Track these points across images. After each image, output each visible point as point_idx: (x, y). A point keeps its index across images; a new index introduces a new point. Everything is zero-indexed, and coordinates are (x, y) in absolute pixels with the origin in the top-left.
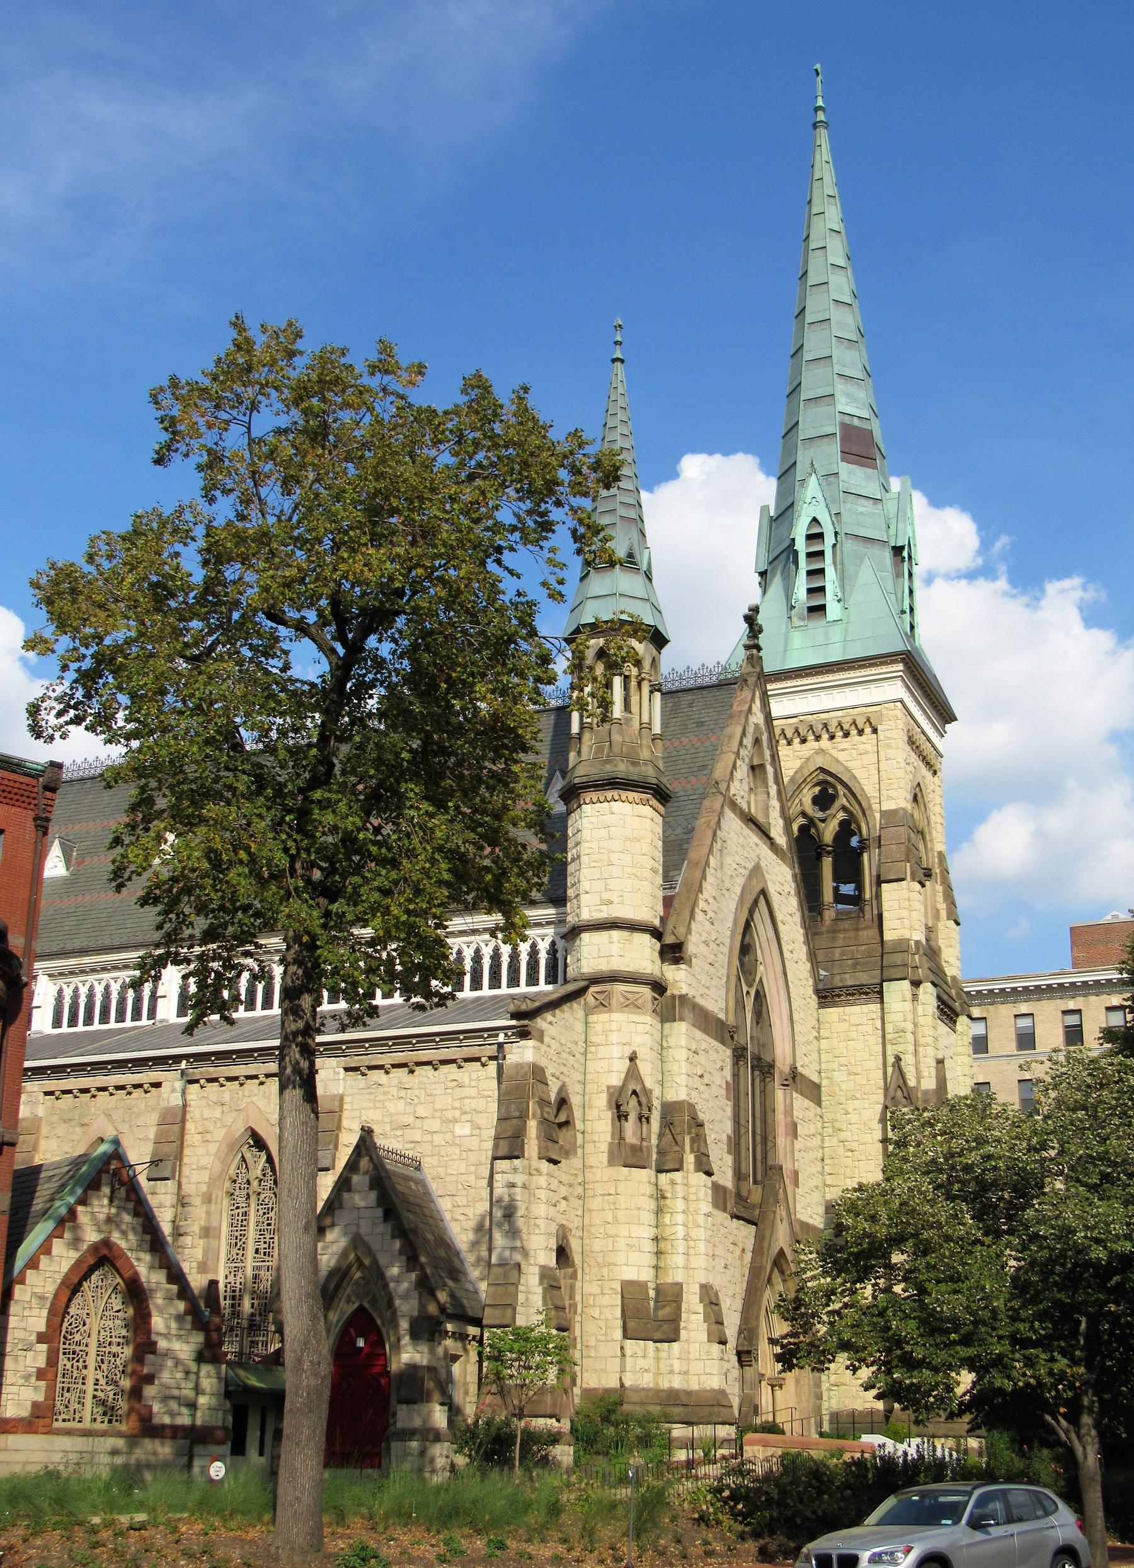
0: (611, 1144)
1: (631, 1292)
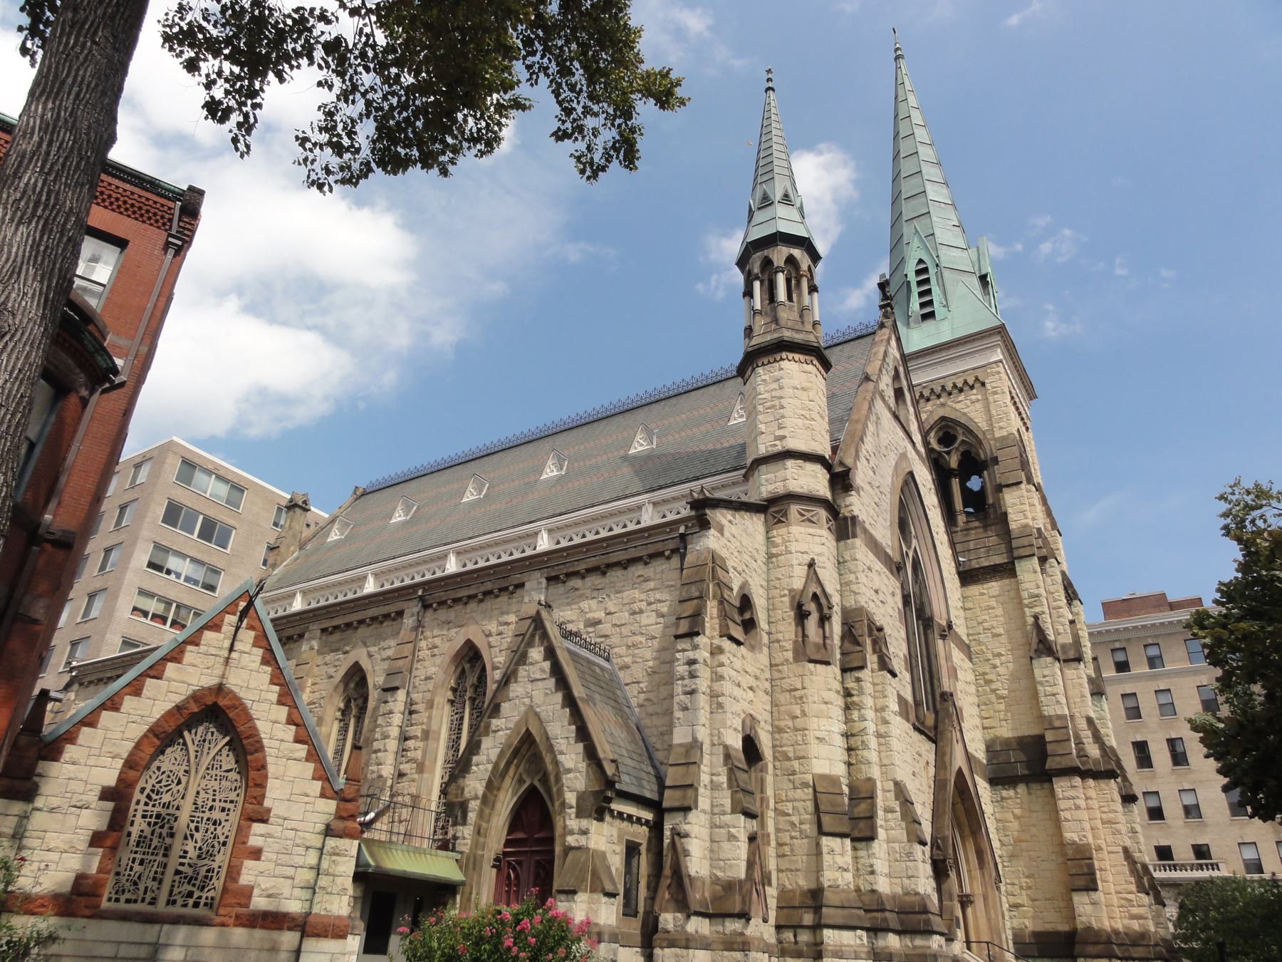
0: (795, 642)
1: (821, 791)
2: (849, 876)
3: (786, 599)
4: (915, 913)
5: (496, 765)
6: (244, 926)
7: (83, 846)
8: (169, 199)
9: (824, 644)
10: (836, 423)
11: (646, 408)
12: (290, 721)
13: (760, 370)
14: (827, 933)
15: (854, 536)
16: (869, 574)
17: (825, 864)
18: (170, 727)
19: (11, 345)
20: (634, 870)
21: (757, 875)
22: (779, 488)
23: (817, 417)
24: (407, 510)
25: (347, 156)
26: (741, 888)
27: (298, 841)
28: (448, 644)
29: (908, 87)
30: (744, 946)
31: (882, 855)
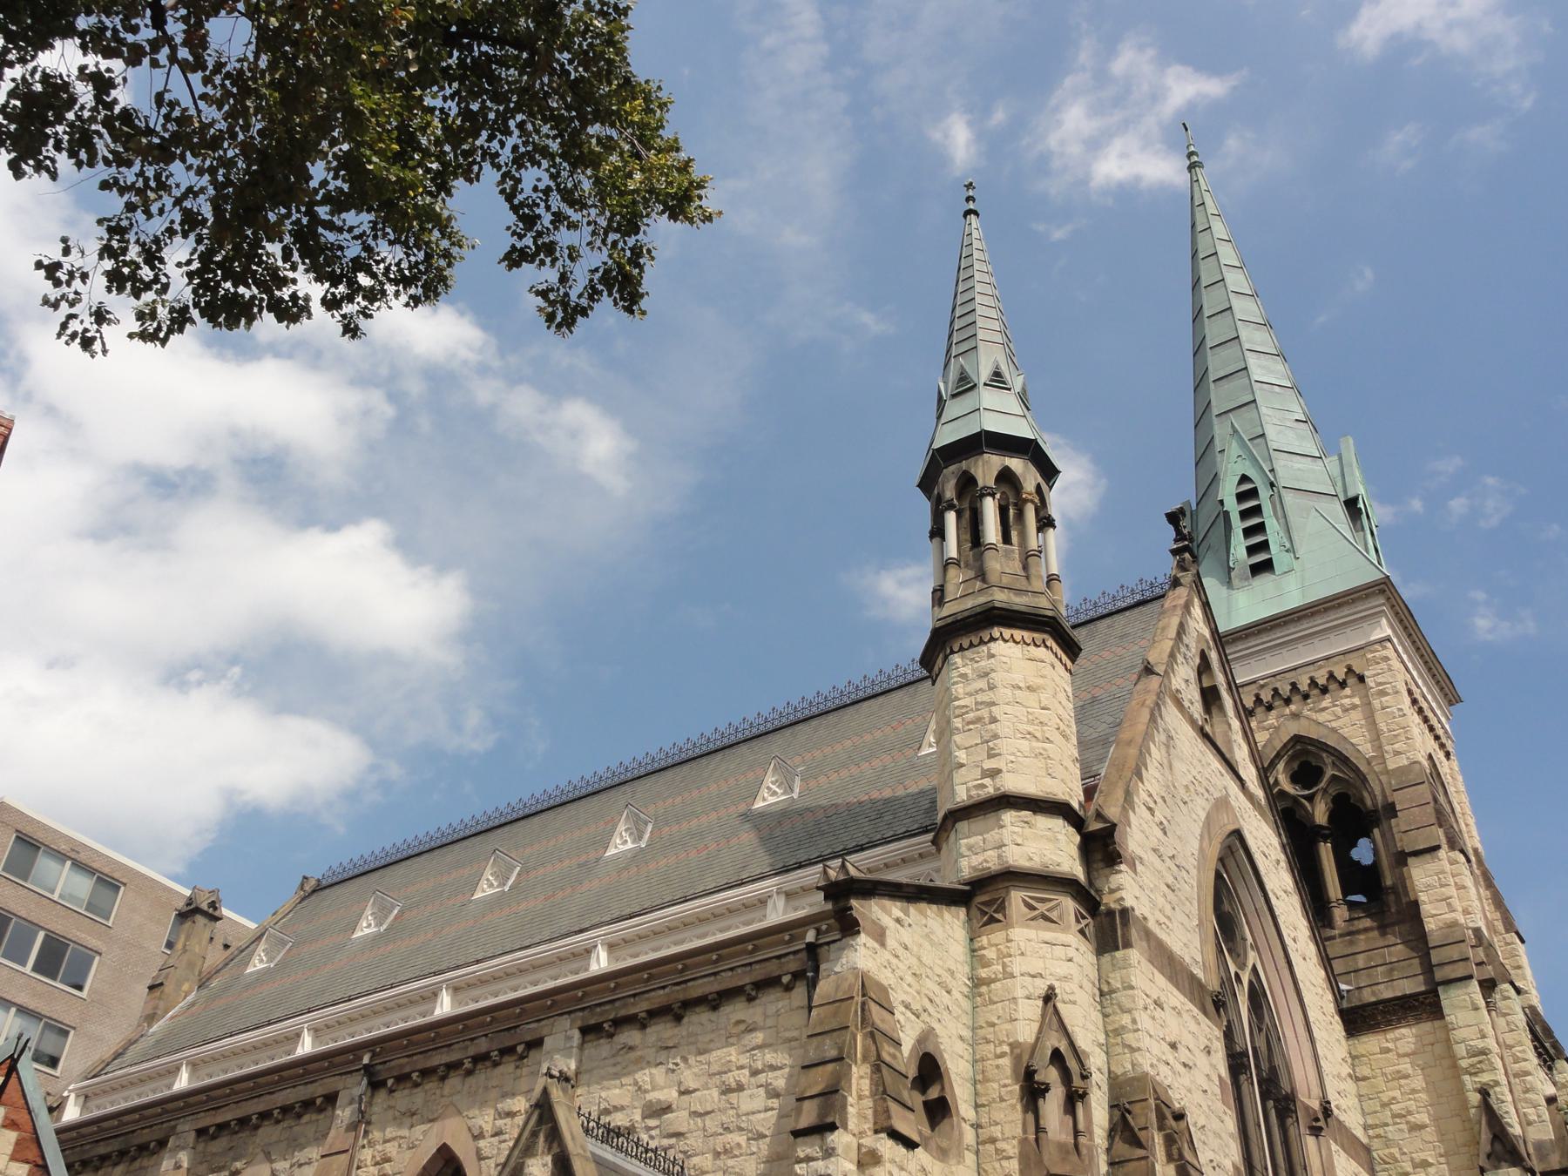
0: (1023, 1142)
3: (1006, 1062)
9: (1076, 1146)
10: (1092, 748)
13: (956, 659)
15: (1128, 945)
16: (1158, 1013)
22: (989, 861)
23: (1056, 737)
24: (381, 913)
25: (149, 296)
28: (408, 1154)
29: (1211, 209)
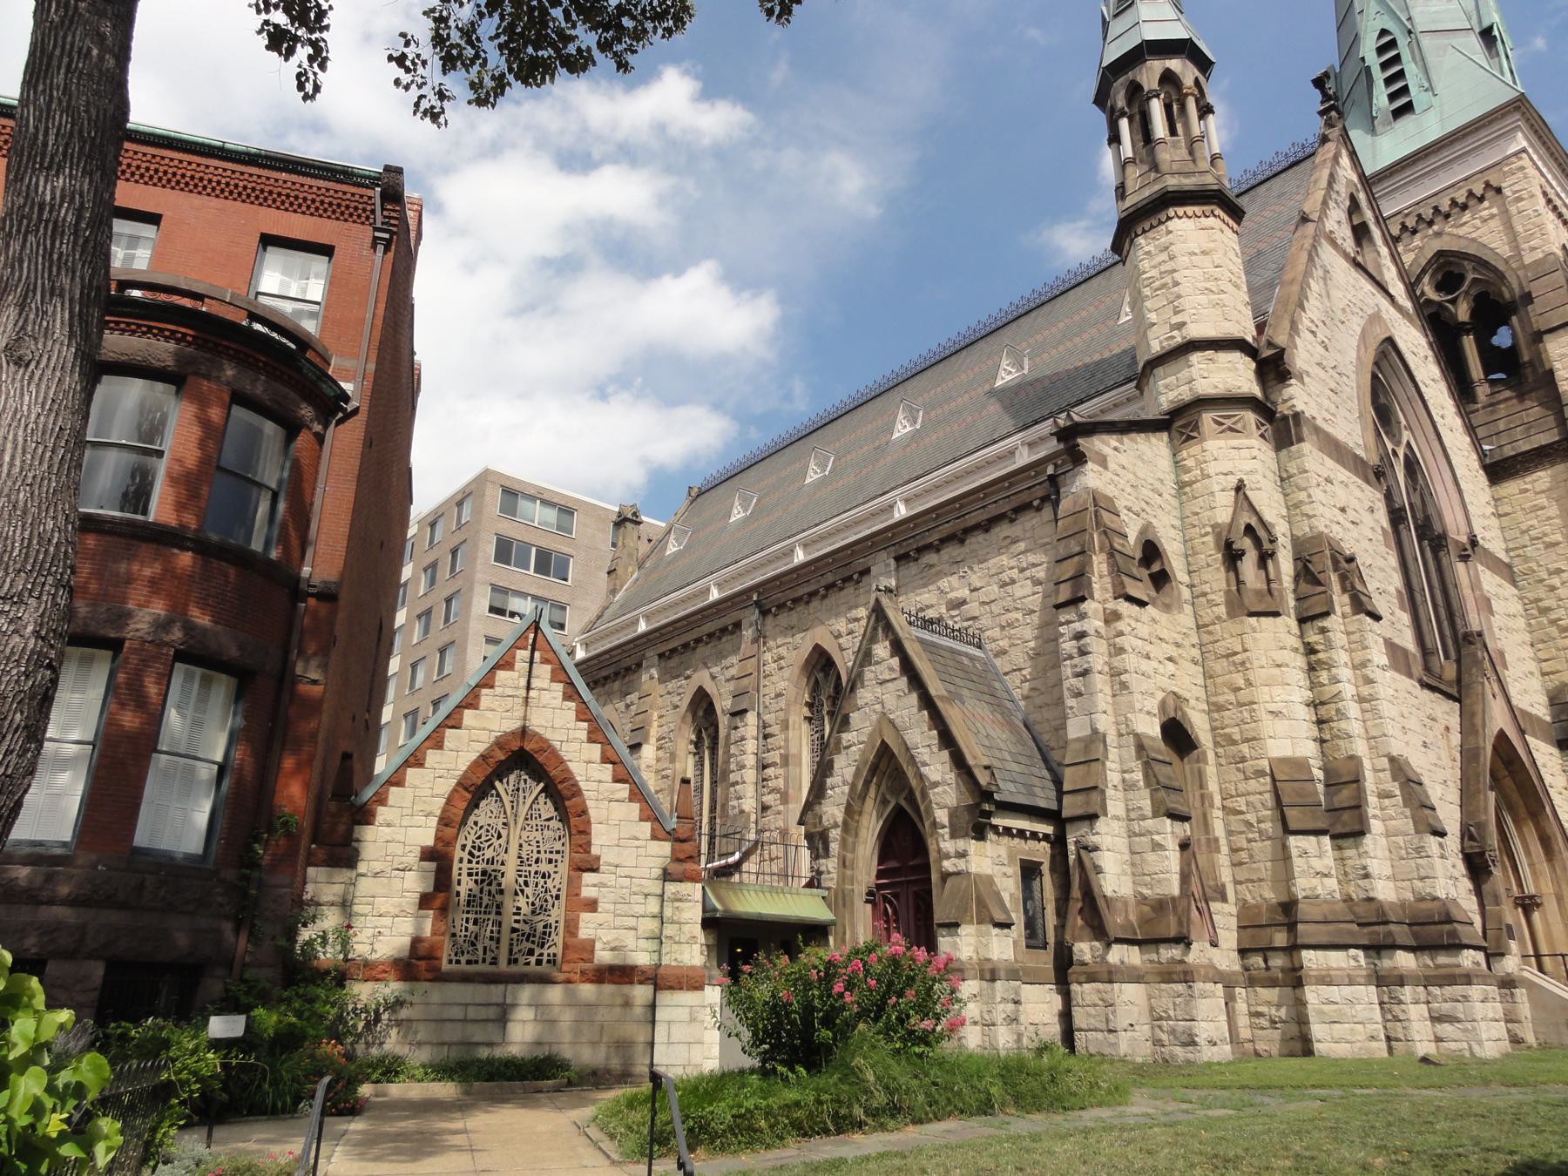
0: (1228, 592)
2: (1332, 883)
3: (1210, 539)
4: (1435, 923)
5: (853, 786)
6: (592, 981)
7: (412, 909)
8: (367, 187)
10: (1259, 293)
11: (1014, 325)
12: (605, 759)
13: (1141, 240)
14: (1308, 956)
15: (1300, 440)
16: (1329, 487)
17: (1296, 869)
18: (478, 779)
19: (38, 373)
20: (1037, 895)
21: (1195, 887)
22: (1184, 394)
23: (1230, 288)
26: (1175, 907)
27: (635, 889)
30: (1187, 976)
31: (1379, 853)
